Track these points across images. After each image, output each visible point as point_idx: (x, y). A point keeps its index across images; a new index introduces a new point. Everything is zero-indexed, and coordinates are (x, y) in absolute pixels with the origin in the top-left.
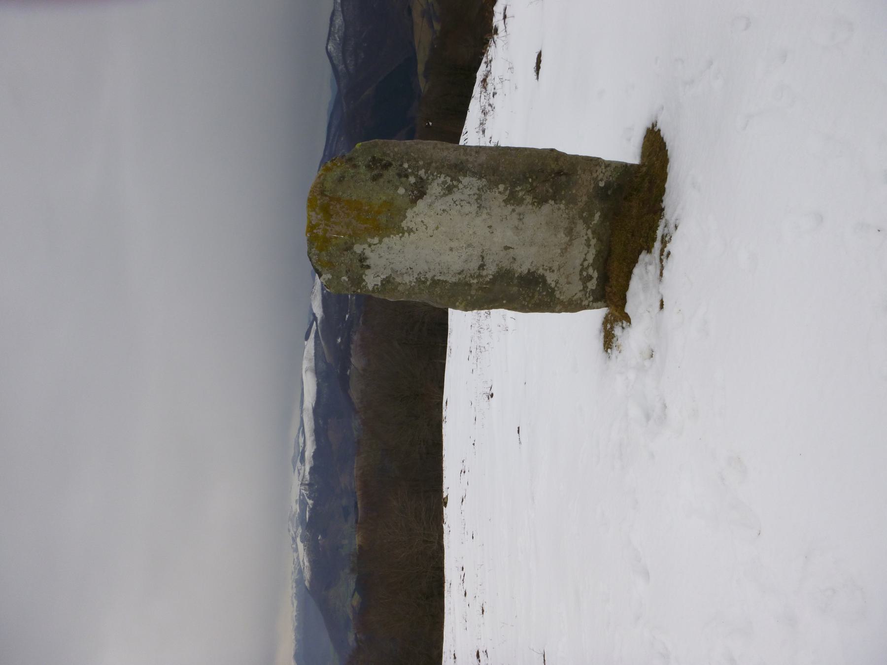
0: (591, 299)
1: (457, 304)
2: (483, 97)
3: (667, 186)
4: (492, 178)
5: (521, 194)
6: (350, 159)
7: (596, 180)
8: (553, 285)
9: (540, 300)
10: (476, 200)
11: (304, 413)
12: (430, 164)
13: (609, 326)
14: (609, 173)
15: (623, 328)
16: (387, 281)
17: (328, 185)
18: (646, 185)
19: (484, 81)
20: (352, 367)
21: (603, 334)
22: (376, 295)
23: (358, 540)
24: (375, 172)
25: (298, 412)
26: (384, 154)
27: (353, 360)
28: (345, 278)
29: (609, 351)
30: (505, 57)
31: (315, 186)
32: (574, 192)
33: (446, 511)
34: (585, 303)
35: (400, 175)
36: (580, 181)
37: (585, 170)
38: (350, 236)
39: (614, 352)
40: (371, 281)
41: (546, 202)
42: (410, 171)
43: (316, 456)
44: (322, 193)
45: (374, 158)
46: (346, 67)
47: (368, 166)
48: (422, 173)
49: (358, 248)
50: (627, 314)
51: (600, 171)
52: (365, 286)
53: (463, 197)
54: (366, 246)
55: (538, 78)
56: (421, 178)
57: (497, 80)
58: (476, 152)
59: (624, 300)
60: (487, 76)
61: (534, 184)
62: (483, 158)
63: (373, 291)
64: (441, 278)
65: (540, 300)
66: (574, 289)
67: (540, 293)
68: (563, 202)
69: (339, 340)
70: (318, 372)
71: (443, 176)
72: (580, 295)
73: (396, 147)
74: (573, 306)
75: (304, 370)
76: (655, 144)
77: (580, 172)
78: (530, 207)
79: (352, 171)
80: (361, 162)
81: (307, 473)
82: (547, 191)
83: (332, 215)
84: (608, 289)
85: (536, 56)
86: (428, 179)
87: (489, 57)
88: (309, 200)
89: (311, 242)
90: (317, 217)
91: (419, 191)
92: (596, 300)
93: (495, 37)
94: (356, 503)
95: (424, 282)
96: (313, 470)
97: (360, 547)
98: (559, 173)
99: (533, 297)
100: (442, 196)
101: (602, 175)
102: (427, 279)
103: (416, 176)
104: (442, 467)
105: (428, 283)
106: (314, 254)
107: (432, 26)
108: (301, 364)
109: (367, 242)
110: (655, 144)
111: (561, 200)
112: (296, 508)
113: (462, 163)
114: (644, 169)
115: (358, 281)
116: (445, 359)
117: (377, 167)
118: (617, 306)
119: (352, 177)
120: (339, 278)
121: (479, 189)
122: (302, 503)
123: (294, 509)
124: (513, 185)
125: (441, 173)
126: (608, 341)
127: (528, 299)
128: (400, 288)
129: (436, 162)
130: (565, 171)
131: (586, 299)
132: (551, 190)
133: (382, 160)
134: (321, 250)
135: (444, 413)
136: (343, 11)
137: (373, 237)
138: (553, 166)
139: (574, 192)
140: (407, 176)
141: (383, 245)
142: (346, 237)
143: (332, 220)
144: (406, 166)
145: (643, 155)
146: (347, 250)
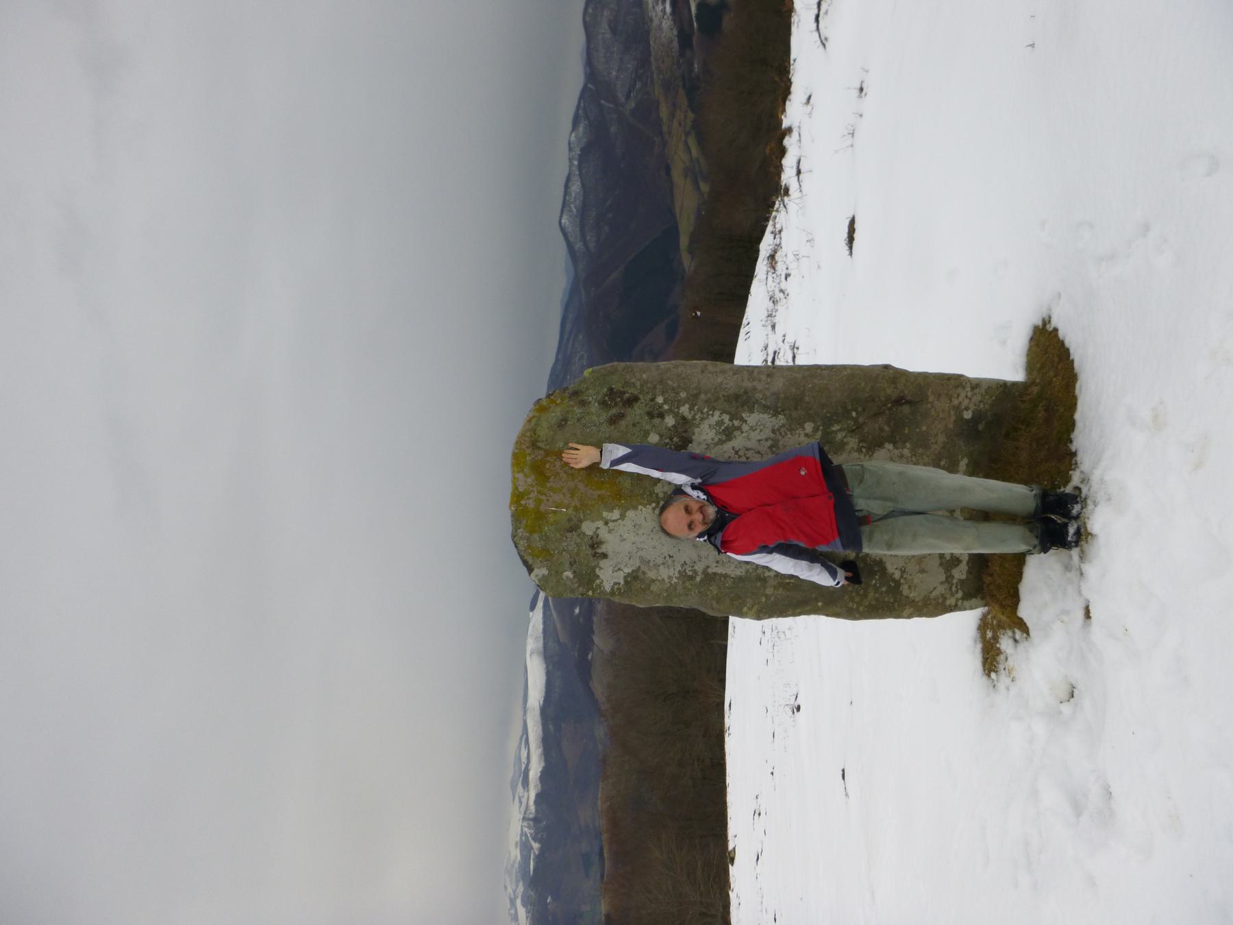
0: (960, 594)
1: (745, 609)
2: (770, 279)
3: (1077, 416)
4: (794, 414)
5: (840, 436)
6: (576, 393)
7: (958, 409)
8: (897, 575)
9: (876, 599)
10: (771, 447)
11: (528, 714)
12: (696, 396)
13: (989, 634)
14: (979, 398)
15: (1016, 641)
16: (634, 578)
17: (543, 432)
18: (1041, 414)
19: (772, 257)
20: (595, 648)
21: (979, 646)
22: (616, 599)
23: (603, 908)
24: (614, 411)
25: (520, 713)
26: (627, 384)
27: (596, 639)
28: (569, 574)
29: (993, 675)
30: (800, 228)
31: (523, 435)
32: (924, 428)
33: (733, 871)
34: (951, 601)
35: (651, 415)
36: (933, 413)
37: (939, 395)
38: (576, 509)
39: (1003, 680)
40: (609, 576)
41: (881, 445)
42: (666, 407)
43: (545, 776)
44: (534, 445)
45: (611, 390)
46: (585, 244)
47: (603, 403)
48: (685, 410)
49: (588, 528)
50: (1021, 619)
51: (963, 395)
52: (599, 586)
53: (749, 444)
54: (600, 524)
55: (851, 254)
56: (684, 418)
57: (791, 257)
58: (768, 376)
59: (1015, 598)
60: (775, 252)
61: (861, 420)
62: (779, 384)
63: (612, 593)
64: (720, 570)
65: (876, 599)
66: (934, 581)
67: (876, 589)
68: (908, 445)
69: (577, 611)
70: (547, 656)
71: (717, 413)
72: (941, 589)
73: (641, 373)
74: (932, 607)
75: (528, 653)
76: (1048, 350)
77: (931, 398)
78: (855, 455)
79: (578, 410)
80: (592, 397)
81: (531, 802)
82: (882, 430)
83: (548, 478)
84: (988, 579)
85: (847, 223)
86: (694, 419)
87: (778, 227)
88: (515, 456)
89: (517, 518)
90: (527, 481)
91: (682, 438)
92: (968, 596)
93: (786, 199)
94: (601, 849)
95: (691, 578)
96: (539, 797)
97: (608, 916)
98: (899, 401)
99: (865, 595)
100: (716, 444)
101: (966, 402)
102: (695, 572)
103: (676, 415)
104: (725, 803)
105: (698, 579)
106: (521, 538)
107: (698, 188)
108: (525, 645)
109: (602, 518)
110: (1048, 350)
111: (905, 442)
112: (516, 854)
113: (746, 392)
114: (1035, 390)
115: (588, 578)
116: (726, 640)
117: (616, 404)
118: (1003, 607)
119: (579, 420)
120: (559, 573)
121: (773, 431)
122: (525, 847)
123: (513, 857)
124: (828, 422)
125: (714, 409)
126: (991, 660)
127: (857, 599)
128: (654, 588)
129: (706, 393)
130: (909, 398)
131: (952, 595)
132: (887, 428)
133: (624, 393)
134: (531, 532)
135: (726, 720)
136: (581, 175)
137: (611, 510)
138: (889, 391)
139: (924, 428)
140: (661, 416)
141: (627, 522)
142: (571, 511)
143: (548, 485)
144: (660, 400)
145: (1030, 367)
146: (571, 530)
